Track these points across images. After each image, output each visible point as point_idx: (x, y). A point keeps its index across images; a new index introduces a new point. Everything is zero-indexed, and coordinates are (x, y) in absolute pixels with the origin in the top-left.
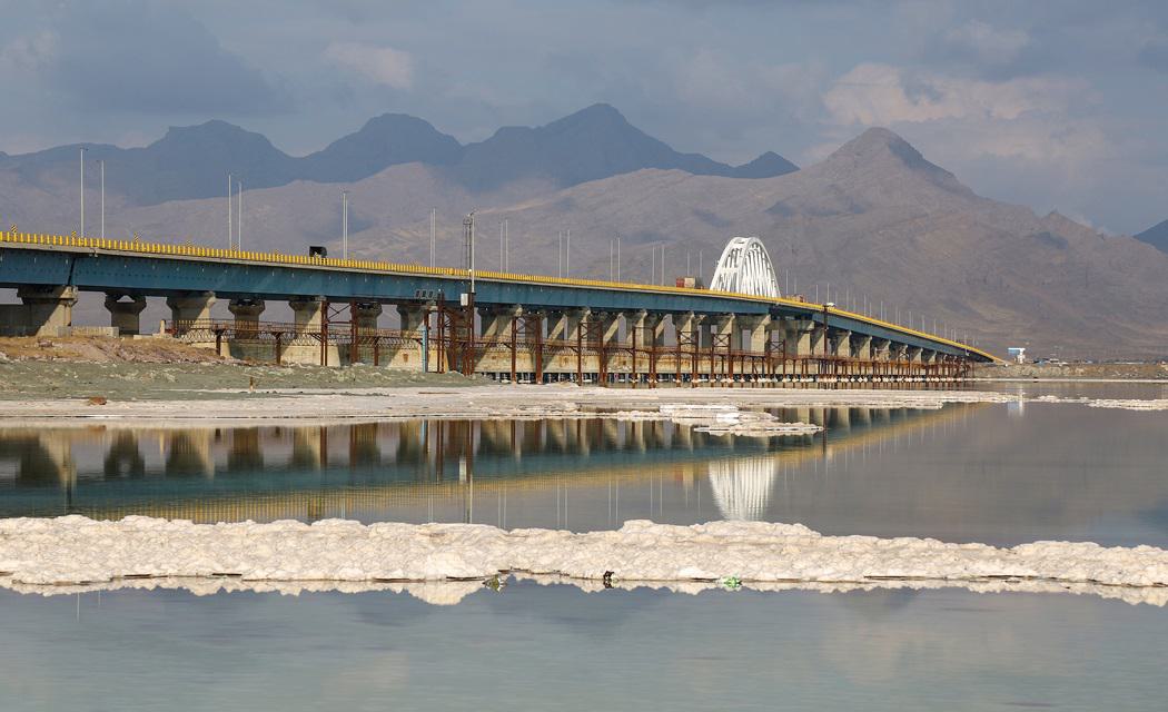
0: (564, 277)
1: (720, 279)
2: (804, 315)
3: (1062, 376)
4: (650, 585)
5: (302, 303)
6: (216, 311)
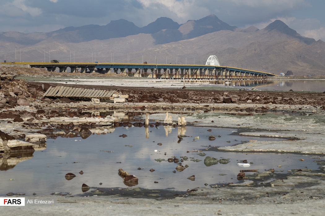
0: (202, 64)
1: (208, 63)
2: (224, 68)
3: (285, 79)
4: (168, 104)
5: (137, 69)
6: (126, 70)
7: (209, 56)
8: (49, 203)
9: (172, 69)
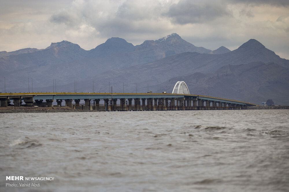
7: (176, 82)
8: (42, 178)
9: (130, 99)
